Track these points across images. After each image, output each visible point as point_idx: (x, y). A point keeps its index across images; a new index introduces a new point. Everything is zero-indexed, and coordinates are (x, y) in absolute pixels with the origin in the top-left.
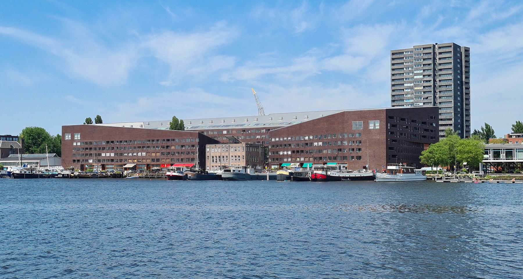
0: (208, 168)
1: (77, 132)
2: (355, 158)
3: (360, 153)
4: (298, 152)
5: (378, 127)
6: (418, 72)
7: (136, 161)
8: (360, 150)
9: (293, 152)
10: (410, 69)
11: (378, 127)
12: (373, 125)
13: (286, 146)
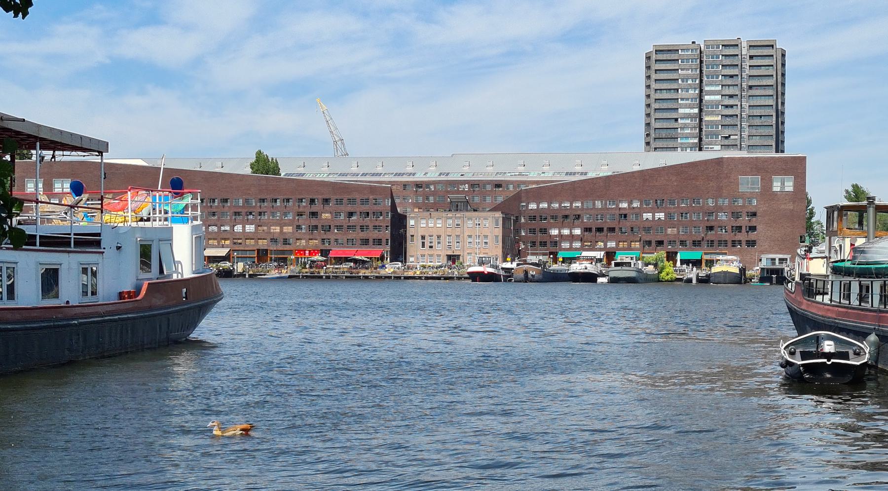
0: (412, 259)
1: (62, 176)
2: (744, 243)
3: (752, 236)
4: (600, 230)
5: (791, 189)
6: (713, 88)
7: (228, 242)
8: (753, 229)
9: (588, 230)
10: (690, 82)
11: (791, 189)
12: (779, 184)
13: (567, 218)
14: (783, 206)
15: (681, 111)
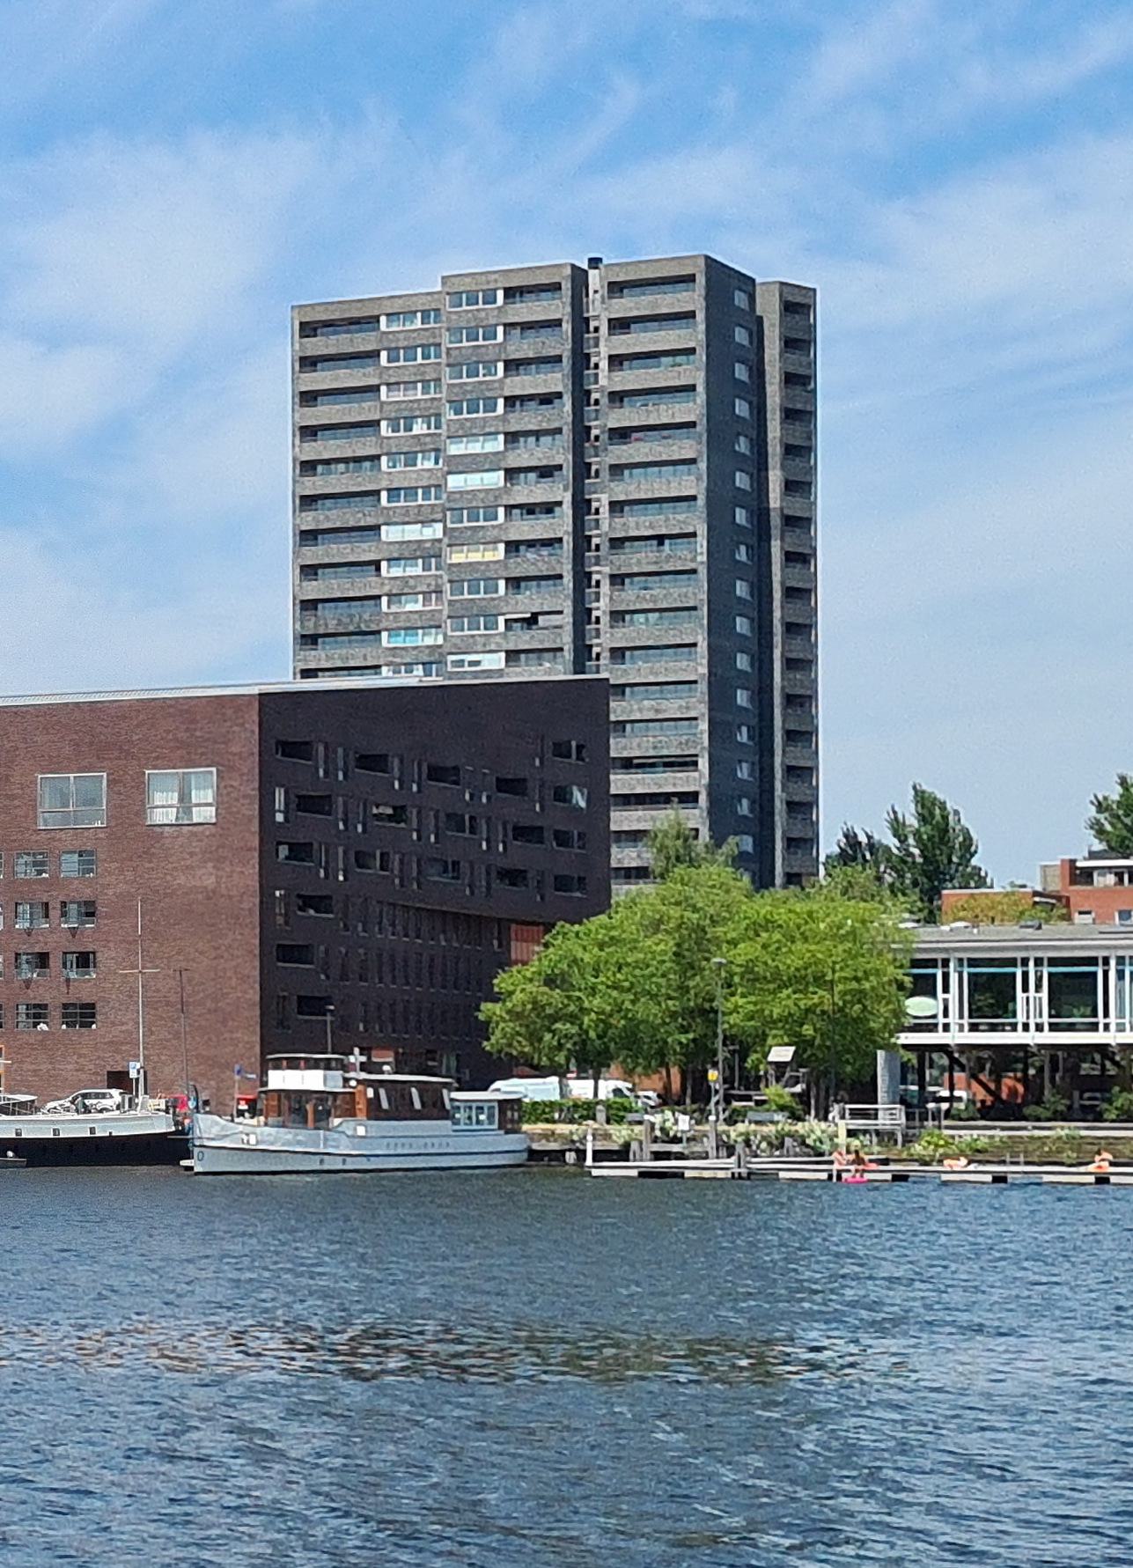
6: (475, 447)
10: (419, 428)
14: (182, 880)
15: (390, 534)
